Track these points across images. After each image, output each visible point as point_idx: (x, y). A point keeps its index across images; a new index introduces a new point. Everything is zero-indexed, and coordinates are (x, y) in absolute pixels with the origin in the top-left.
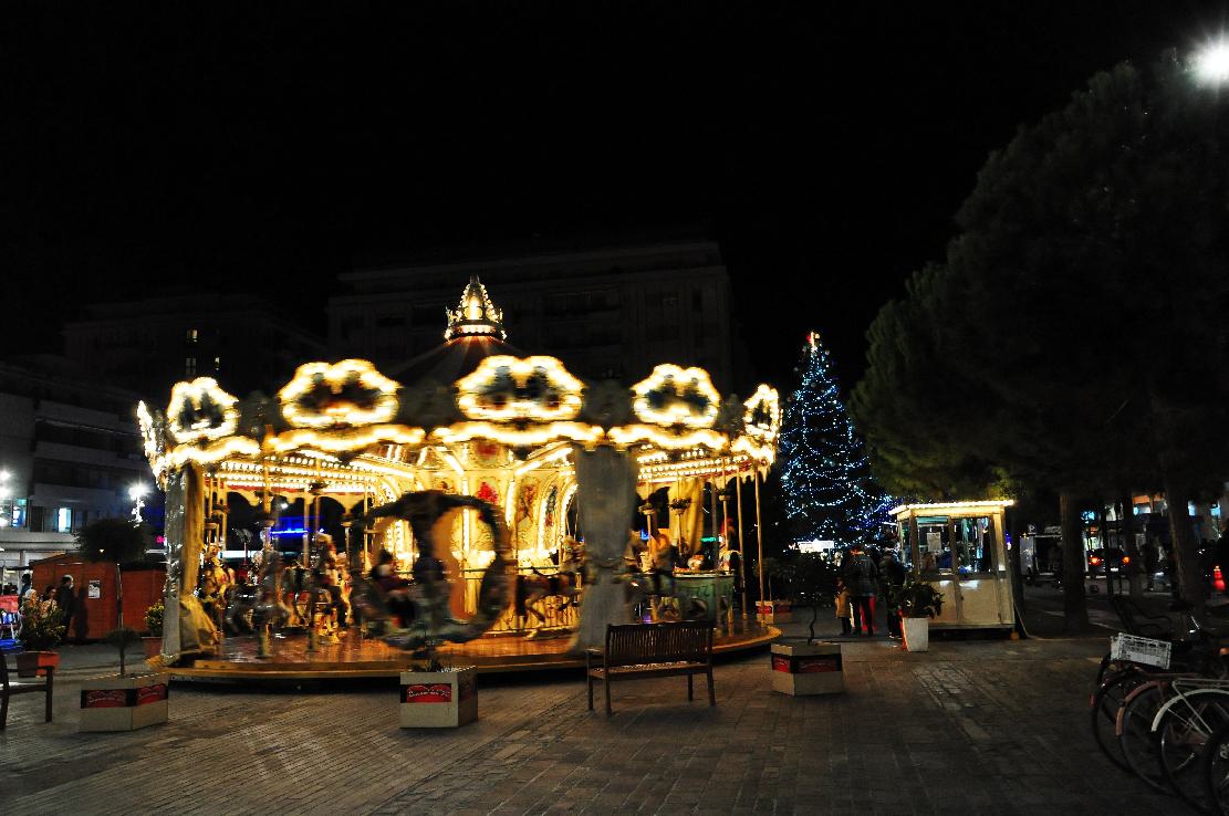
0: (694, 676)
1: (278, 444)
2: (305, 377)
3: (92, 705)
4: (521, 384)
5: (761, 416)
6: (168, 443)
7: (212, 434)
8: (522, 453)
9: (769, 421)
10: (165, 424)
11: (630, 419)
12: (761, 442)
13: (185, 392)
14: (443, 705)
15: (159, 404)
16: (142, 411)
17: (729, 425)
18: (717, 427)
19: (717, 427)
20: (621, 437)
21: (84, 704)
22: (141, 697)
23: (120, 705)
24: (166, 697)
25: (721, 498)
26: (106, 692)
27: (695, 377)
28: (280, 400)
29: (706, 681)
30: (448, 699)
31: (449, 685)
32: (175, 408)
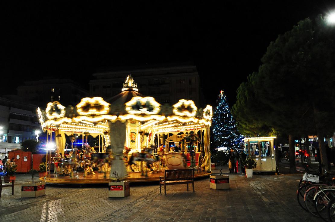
0: (189, 184)
1: (123, 118)
2: (85, 101)
3: (24, 191)
4: (93, 105)
6: (46, 119)
7: (148, 113)
10: (45, 114)
11: (125, 113)
12: (208, 120)
13: (50, 105)
14: (121, 191)
15: (43, 108)
16: (39, 110)
17: (199, 116)
18: (196, 117)
19: (196, 117)
21: (22, 190)
22: (38, 188)
23: (32, 190)
24: (45, 188)
25: (161, 138)
26: (29, 187)
27: (190, 103)
28: (125, 106)
29: (192, 185)
30: (122, 190)
31: (122, 186)
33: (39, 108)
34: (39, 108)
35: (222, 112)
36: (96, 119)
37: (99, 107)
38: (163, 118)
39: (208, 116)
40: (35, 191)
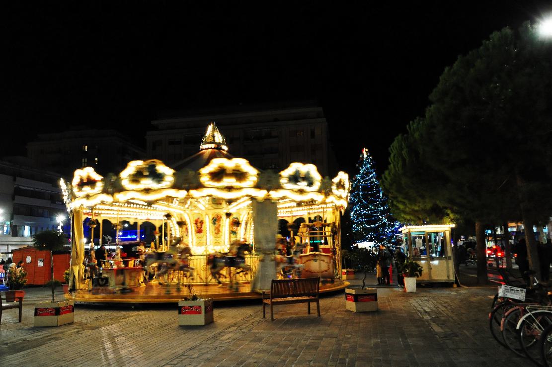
5: (340, 185)
6: (73, 196)
8: (230, 202)
9: (343, 187)
11: (279, 187)
12: (340, 197)
13: (81, 174)
15: (69, 179)
16: (62, 182)
17: (326, 190)
20: (274, 195)
21: (36, 314)
23: (52, 314)
24: (73, 311)
26: (46, 309)
28: (200, 174)
30: (200, 313)
31: (200, 307)
32: (76, 181)
33: (62, 179)
34: (62, 179)
35: (365, 183)
36: (151, 197)
37: (240, 175)
38: (108, 198)
39: (341, 190)
40: (56, 317)
